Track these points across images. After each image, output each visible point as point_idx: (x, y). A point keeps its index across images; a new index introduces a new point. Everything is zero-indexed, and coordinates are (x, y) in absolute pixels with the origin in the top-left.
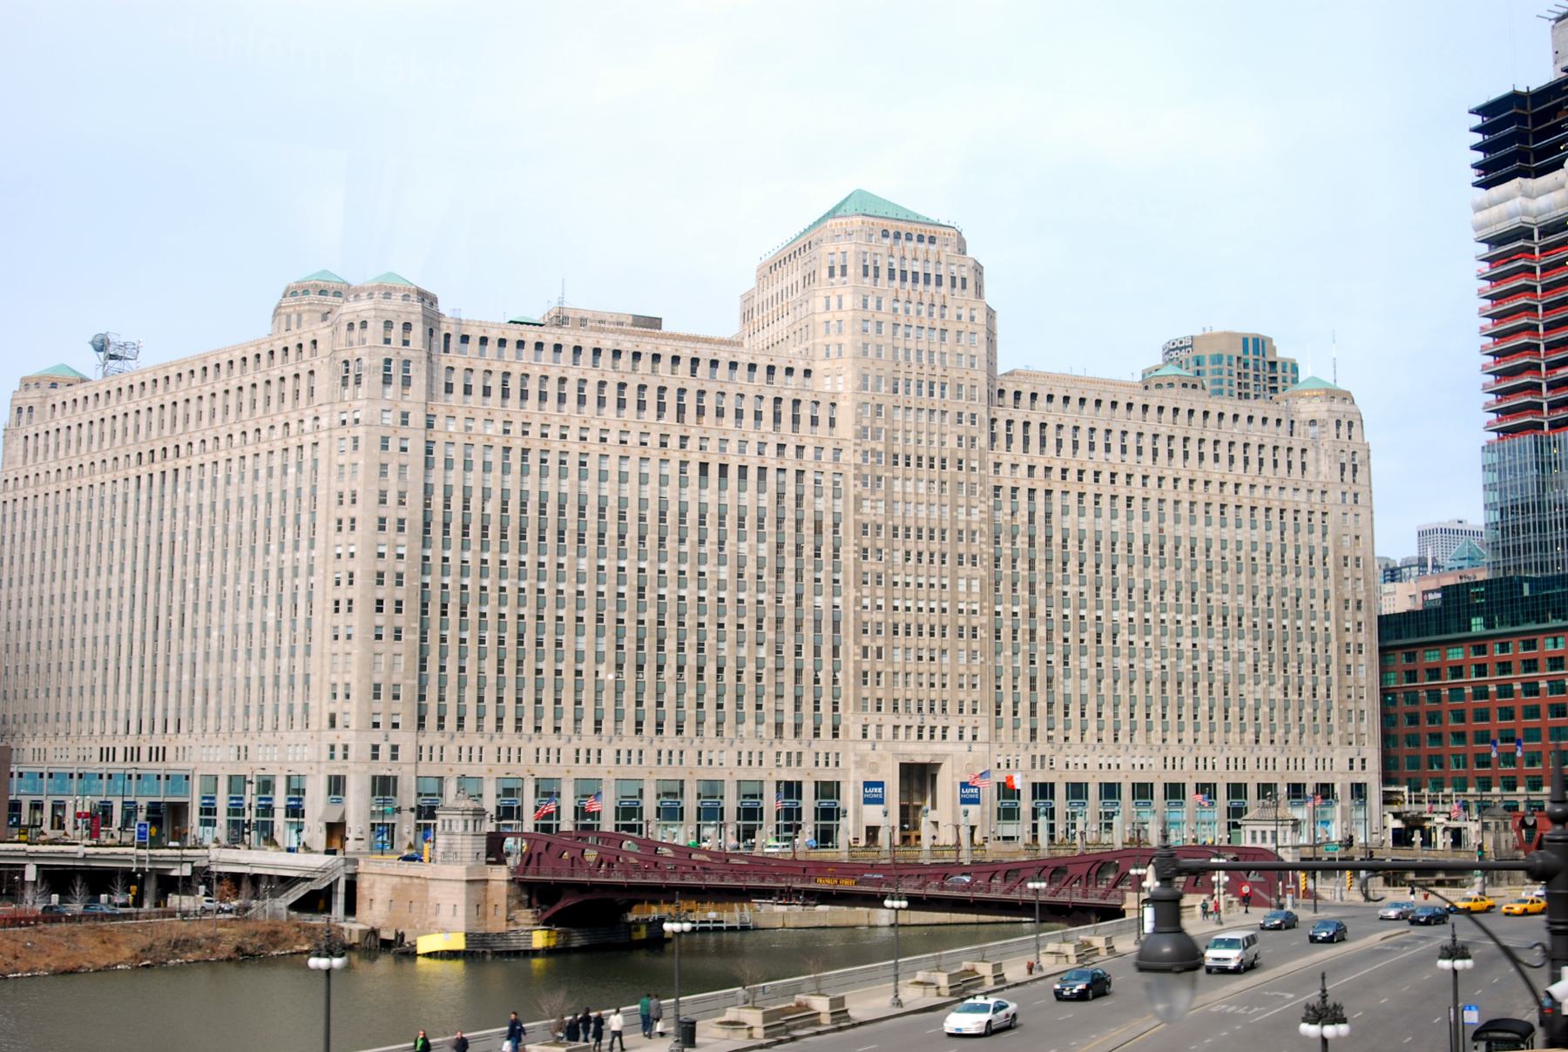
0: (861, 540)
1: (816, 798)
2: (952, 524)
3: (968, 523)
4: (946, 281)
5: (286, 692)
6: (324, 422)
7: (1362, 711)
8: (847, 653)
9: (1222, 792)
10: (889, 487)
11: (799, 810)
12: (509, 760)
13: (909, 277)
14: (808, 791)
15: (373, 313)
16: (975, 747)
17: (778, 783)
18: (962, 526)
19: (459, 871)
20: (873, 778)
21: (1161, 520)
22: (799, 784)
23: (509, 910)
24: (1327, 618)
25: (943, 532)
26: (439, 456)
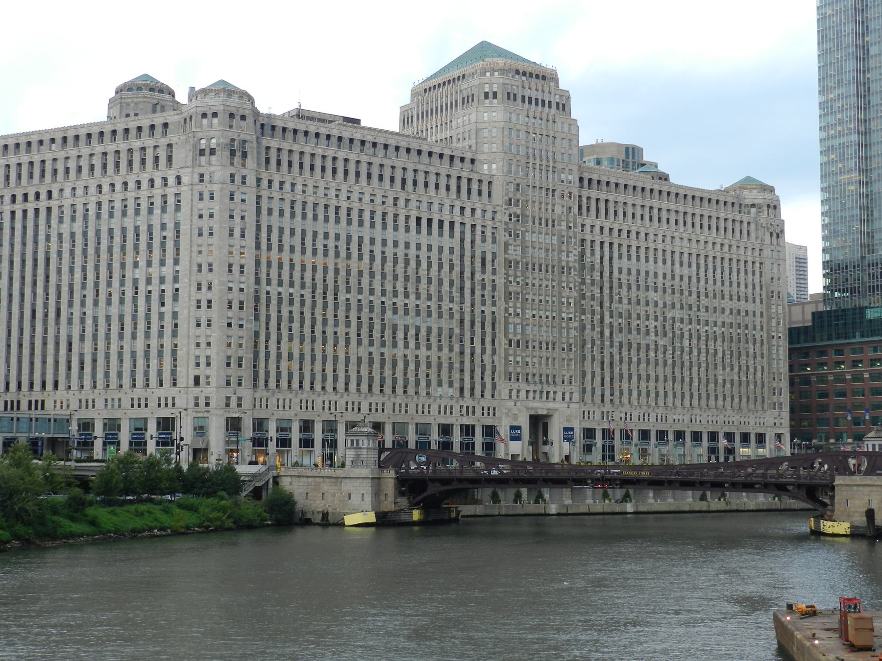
0: (508, 271)
1: (483, 436)
2: (558, 262)
3: (568, 262)
4: (554, 106)
5: (155, 361)
6: (185, 180)
7: (781, 389)
8: (500, 343)
9: (705, 437)
10: (523, 238)
11: (473, 444)
12: (307, 408)
13: (533, 102)
14: (478, 431)
15: (222, 107)
16: (572, 405)
17: (461, 425)
18: (564, 264)
19: (365, 472)
20: (515, 424)
21: (673, 264)
22: (473, 426)
23: (395, 498)
24: (762, 329)
25: (553, 267)
26: (264, 207)
